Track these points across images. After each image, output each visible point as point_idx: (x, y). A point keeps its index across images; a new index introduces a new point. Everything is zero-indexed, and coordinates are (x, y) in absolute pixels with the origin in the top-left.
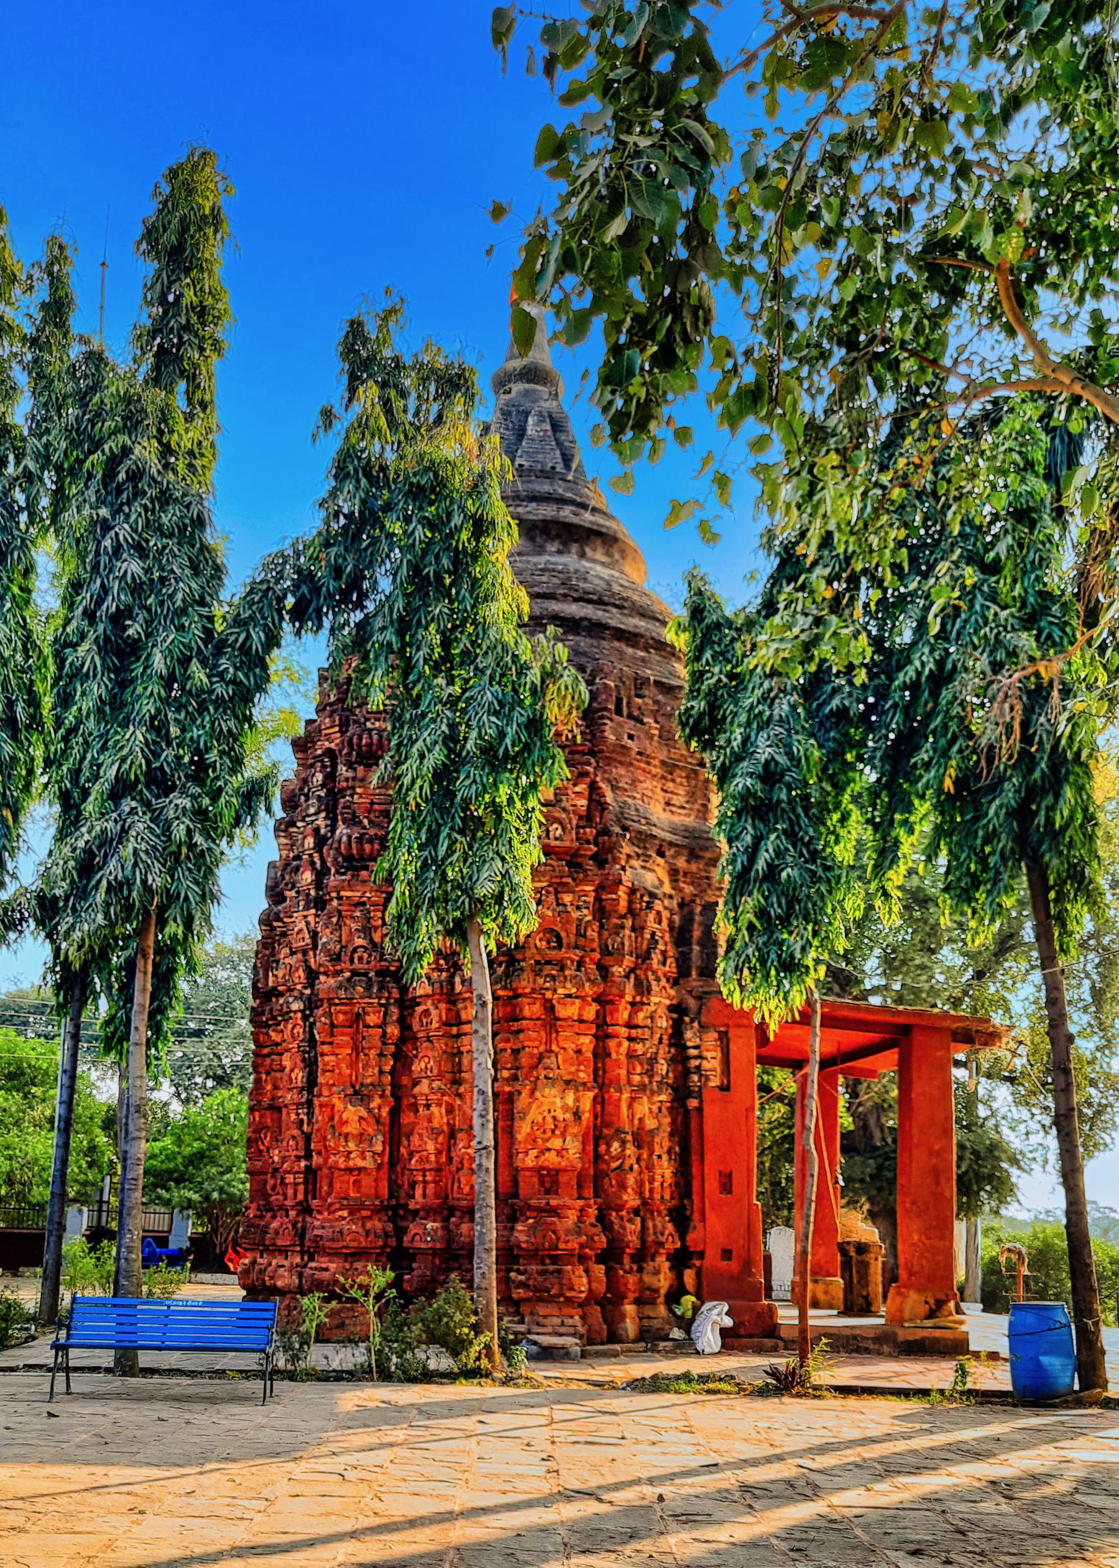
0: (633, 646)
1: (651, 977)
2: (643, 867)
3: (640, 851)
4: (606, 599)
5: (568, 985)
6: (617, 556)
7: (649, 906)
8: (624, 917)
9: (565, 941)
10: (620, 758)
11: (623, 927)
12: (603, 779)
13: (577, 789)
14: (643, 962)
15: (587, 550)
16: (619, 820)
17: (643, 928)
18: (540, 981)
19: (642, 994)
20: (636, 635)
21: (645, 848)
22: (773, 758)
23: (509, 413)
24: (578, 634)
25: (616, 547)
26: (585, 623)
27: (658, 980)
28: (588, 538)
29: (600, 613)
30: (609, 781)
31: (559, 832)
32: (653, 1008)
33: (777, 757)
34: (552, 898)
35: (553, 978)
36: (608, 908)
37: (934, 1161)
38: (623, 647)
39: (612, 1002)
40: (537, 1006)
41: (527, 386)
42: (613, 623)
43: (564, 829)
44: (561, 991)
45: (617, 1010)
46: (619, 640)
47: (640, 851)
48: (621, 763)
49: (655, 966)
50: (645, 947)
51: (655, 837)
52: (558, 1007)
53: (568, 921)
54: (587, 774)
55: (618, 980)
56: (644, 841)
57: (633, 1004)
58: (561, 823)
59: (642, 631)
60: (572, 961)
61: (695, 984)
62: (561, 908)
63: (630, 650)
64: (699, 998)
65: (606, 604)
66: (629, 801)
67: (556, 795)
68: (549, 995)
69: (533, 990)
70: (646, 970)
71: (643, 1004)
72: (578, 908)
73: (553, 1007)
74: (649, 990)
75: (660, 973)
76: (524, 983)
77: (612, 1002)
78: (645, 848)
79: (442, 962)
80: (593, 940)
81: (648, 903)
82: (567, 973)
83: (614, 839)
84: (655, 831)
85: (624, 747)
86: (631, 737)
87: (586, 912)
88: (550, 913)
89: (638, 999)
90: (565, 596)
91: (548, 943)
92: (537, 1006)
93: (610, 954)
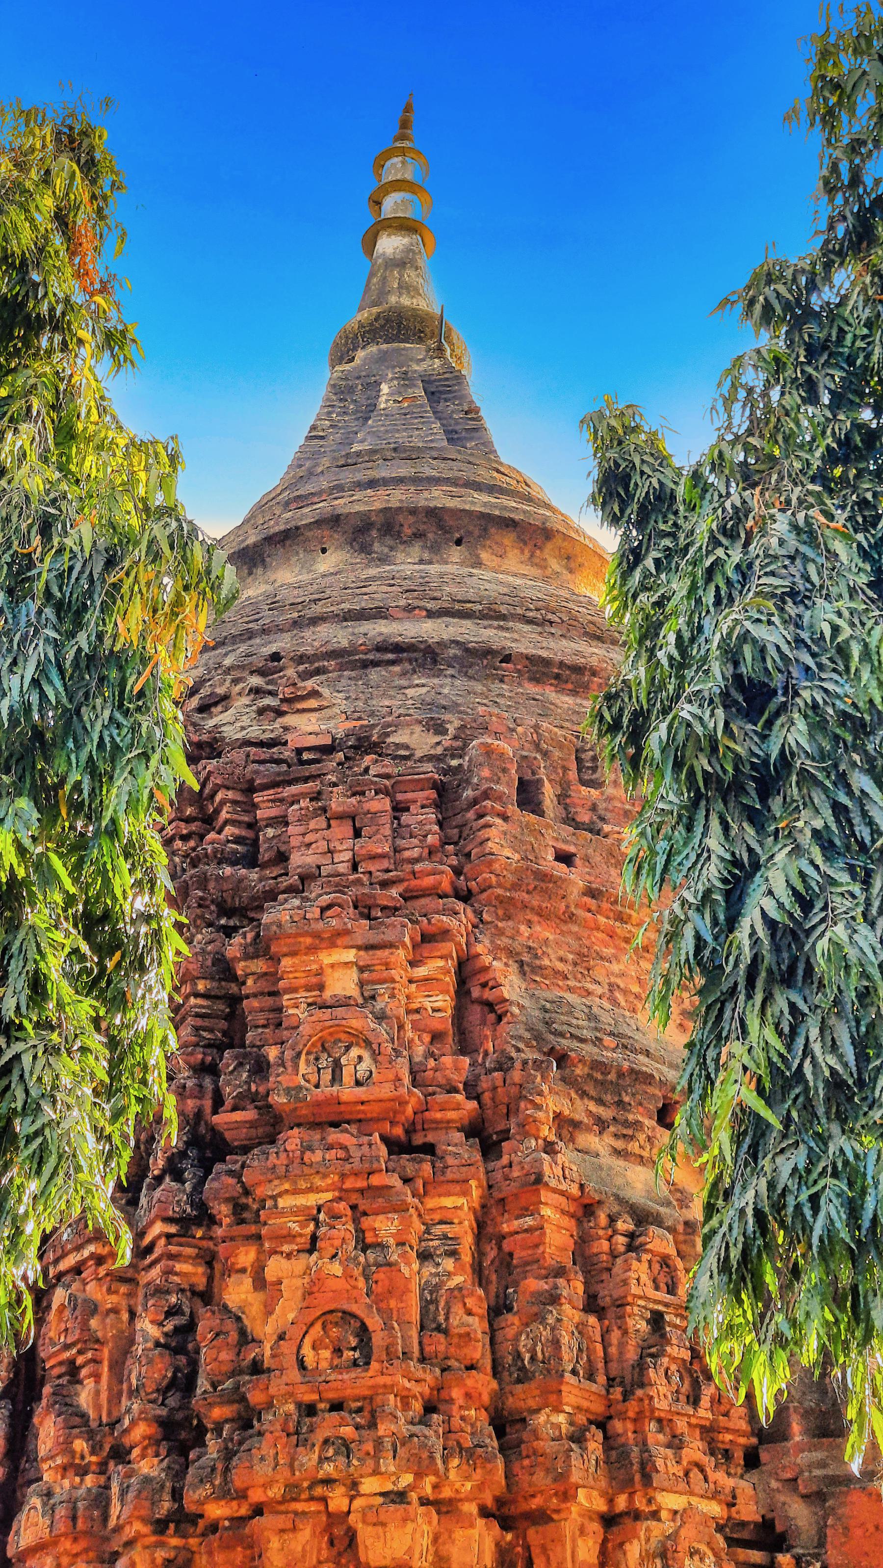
0: (574, 693)
1: (655, 1437)
2: (617, 1153)
3: (606, 1113)
4: (503, 609)
5: (388, 1465)
6: (555, 565)
7: (634, 1245)
8: (560, 1272)
9: (378, 1339)
10: (535, 901)
11: (554, 1299)
12: (495, 951)
13: (421, 971)
14: (626, 1396)
15: (484, 555)
16: (538, 1037)
17: (621, 1304)
18: (308, 1459)
19: (626, 1485)
20: (578, 669)
21: (620, 1104)
22: (745, 637)
23: (351, 390)
24: (439, 674)
25: (549, 546)
26: (453, 651)
27: (676, 1443)
28: (484, 533)
29: (491, 632)
30: (510, 953)
31: (367, 1064)
32: (669, 1527)
33: (760, 632)
34: (345, 1229)
35: (346, 1448)
36: (520, 1255)
37: (392, 1241)
38: (550, 693)
39: (542, 1517)
40: (305, 1534)
41: (384, 346)
42: (522, 647)
43: (376, 1055)
44: (370, 1485)
45: (559, 1540)
46: (536, 679)
47: (606, 1113)
48: (543, 915)
49: (662, 1405)
50: (632, 1354)
51: (648, 1079)
52: (365, 1534)
53: (397, 1290)
54: (445, 934)
55: (548, 1446)
56: (618, 1089)
57: (609, 1521)
58: (368, 1043)
59: (594, 662)
60: (405, 1401)
61: (804, 1458)
62: (371, 1255)
63: (567, 701)
64: (816, 1498)
65: (503, 617)
66: (570, 997)
67: (361, 984)
68: (338, 1500)
69: (292, 1493)
70: (638, 1419)
71: (637, 1516)
72: (425, 1256)
73: (352, 1537)
74: (647, 1472)
75: (681, 1425)
76: (263, 1470)
77: (542, 1517)
78: (620, 1104)
79: (80, 1445)
80: (467, 1337)
81: (631, 1236)
82: (383, 1429)
83: (516, 1075)
84: (644, 1064)
85: (544, 877)
86: (565, 858)
87: (448, 1264)
88: (336, 1269)
89: (622, 1503)
90: (409, 609)
91: (338, 1352)
92: (305, 1534)
93: (524, 1377)
